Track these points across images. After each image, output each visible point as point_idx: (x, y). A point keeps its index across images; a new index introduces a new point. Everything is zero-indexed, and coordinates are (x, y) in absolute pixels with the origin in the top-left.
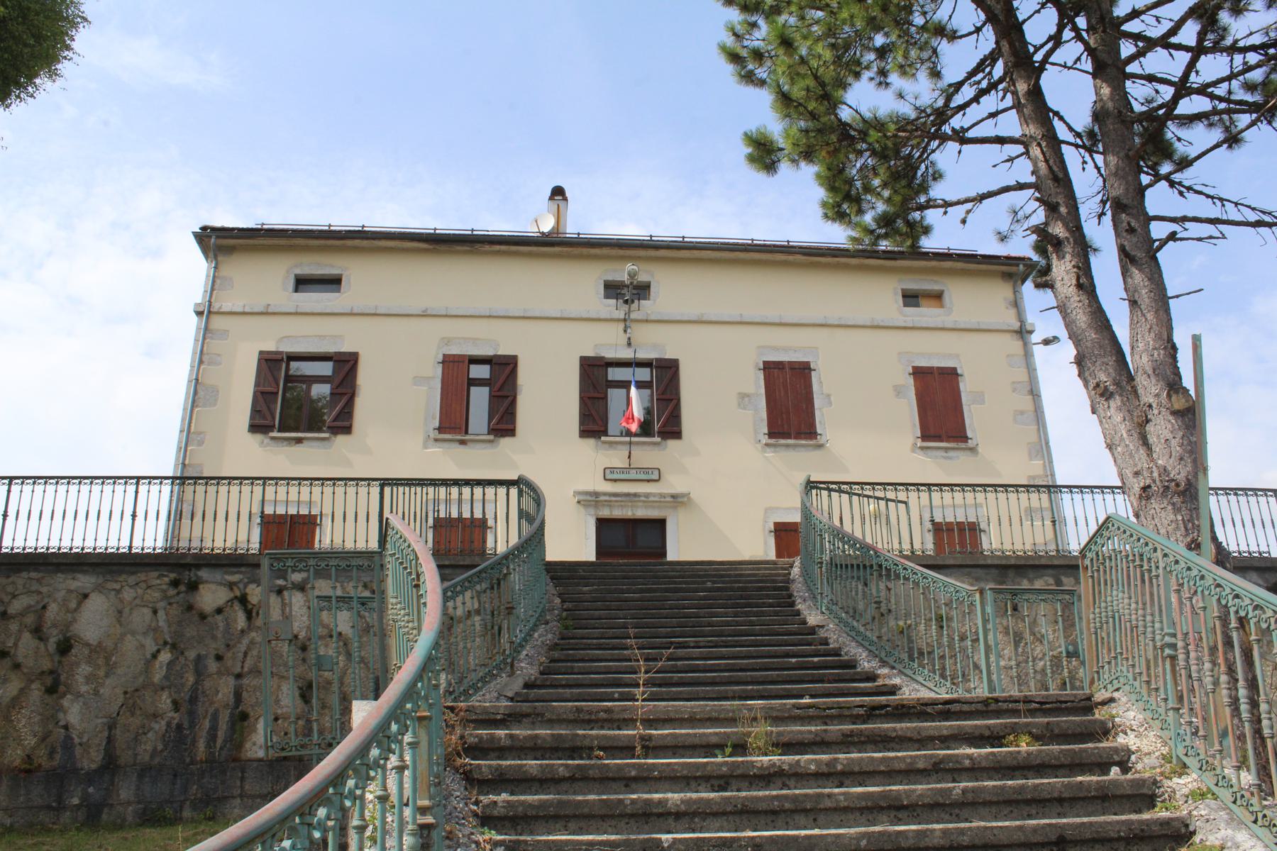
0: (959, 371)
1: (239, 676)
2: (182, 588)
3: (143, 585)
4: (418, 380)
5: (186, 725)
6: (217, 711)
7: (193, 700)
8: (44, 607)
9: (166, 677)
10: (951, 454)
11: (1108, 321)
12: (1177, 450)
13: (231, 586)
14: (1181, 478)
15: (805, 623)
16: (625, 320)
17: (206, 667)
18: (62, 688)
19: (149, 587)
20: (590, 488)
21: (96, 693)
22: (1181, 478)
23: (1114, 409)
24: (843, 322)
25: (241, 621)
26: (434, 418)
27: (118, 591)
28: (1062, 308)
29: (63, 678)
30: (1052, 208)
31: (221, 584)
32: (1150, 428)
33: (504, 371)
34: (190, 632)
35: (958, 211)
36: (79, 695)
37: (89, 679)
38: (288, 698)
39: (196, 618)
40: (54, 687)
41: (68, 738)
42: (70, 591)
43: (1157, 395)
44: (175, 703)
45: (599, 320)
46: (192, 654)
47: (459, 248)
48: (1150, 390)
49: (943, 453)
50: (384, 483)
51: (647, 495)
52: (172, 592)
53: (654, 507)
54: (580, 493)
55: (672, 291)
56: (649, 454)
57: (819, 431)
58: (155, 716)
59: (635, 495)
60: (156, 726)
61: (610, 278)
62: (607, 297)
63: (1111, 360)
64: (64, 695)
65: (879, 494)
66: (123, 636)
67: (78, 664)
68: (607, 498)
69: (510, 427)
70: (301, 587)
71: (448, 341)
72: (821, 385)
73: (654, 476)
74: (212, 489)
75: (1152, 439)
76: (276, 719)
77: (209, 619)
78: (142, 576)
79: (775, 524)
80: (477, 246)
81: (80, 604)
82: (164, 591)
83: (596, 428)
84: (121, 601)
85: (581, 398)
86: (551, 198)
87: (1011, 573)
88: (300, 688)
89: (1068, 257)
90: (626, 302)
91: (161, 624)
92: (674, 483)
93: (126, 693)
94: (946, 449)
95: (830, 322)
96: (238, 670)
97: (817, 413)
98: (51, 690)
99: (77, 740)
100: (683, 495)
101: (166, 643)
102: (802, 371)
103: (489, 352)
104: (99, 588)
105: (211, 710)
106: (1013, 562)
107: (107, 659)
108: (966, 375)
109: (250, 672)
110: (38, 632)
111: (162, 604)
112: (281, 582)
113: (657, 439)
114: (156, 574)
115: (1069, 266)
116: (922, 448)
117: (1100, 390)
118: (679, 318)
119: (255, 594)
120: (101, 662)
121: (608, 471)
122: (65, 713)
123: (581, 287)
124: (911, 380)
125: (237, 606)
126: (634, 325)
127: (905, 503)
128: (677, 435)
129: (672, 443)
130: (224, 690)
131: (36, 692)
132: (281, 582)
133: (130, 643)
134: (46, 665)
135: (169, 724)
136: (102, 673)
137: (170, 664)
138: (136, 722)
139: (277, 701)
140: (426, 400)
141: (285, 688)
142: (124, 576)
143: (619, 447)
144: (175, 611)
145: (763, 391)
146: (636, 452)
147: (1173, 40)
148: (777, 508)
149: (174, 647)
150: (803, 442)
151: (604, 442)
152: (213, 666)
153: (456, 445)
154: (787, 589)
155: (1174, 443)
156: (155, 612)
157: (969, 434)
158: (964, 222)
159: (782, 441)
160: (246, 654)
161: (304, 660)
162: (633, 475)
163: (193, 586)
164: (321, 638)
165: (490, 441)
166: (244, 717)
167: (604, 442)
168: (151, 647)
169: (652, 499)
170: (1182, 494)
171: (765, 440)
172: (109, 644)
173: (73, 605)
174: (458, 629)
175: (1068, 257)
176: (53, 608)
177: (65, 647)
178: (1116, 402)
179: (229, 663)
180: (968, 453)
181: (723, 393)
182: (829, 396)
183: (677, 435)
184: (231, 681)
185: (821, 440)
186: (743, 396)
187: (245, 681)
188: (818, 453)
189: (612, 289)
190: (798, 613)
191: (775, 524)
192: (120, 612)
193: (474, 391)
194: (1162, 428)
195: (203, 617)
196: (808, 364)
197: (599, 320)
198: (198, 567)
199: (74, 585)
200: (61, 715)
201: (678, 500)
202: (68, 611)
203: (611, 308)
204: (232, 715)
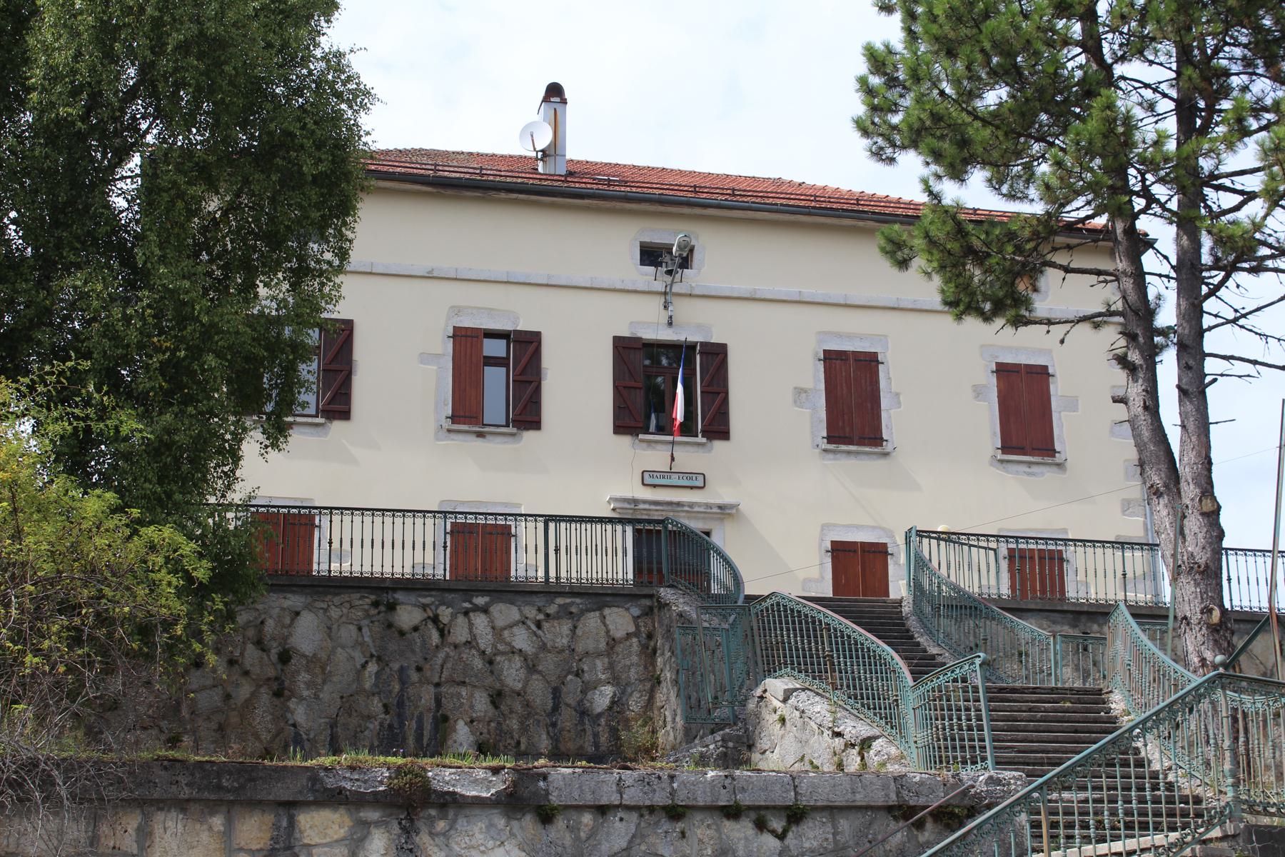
0: (1051, 371)
1: (437, 685)
2: (382, 608)
3: (347, 605)
4: (425, 358)
5: (396, 725)
6: (421, 713)
7: (401, 704)
8: (262, 623)
9: (376, 685)
10: (1035, 469)
11: (1165, 435)
12: (1202, 541)
13: (424, 607)
14: (1202, 562)
15: (925, 651)
16: (665, 293)
17: (408, 676)
18: (287, 693)
19: (352, 607)
20: (629, 495)
21: (317, 697)
22: (1202, 562)
23: (1162, 508)
24: (919, 307)
25: (435, 637)
26: (446, 405)
27: (325, 610)
28: (1132, 422)
29: (287, 683)
30: (1131, 337)
31: (415, 605)
32: (1186, 521)
33: (525, 350)
34: (392, 646)
35: (1058, 331)
36: (302, 699)
37: (309, 685)
38: (481, 703)
39: (396, 634)
40: (280, 693)
41: (297, 735)
42: (283, 609)
43: (1192, 500)
44: (385, 706)
45: (636, 292)
46: (396, 666)
47: (469, 194)
48: (1189, 491)
49: (1024, 468)
50: (548, 519)
51: (691, 505)
52: (373, 611)
53: (696, 518)
54: (616, 500)
55: (723, 257)
56: (692, 456)
57: (885, 437)
58: (369, 717)
59: (679, 504)
60: (371, 726)
61: (647, 240)
62: (643, 263)
63: (1163, 467)
64: (289, 699)
65: (982, 544)
66: (334, 648)
67: (298, 672)
68: (647, 506)
69: (535, 419)
70: (485, 610)
71: (457, 310)
72: (891, 380)
73: (697, 482)
74: (378, 520)
75: (1187, 531)
76: (472, 721)
77: (408, 636)
78: (346, 597)
79: (833, 542)
80: (492, 193)
81: (293, 620)
82: (366, 611)
83: (633, 424)
84: (330, 618)
85: (616, 388)
86: (546, 99)
87: (1083, 618)
88: (491, 696)
89: (1140, 381)
90: (669, 272)
91: (366, 639)
92: (719, 493)
93: (342, 697)
94: (1030, 464)
95: (903, 305)
96: (436, 680)
97: (884, 415)
98: (278, 694)
99: (304, 737)
100: (732, 506)
101: (372, 656)
102: (868, 364)
103: (506, 326)
104: (308, 607)
105: (416, 714)
106: (1085, 609)
107: (323, 669)
108: (1058, 375)
109: (447, 682)
110: (259, 643)
111: (366, 622)
112: (467, 605)
113: (700, 439)
114: (358, 595)
115: (1140, 389)
116: (1002, 461)
117: (1153, 490)
118: (728, 294)
119: (445, 613)
120: (317, 670)
121: (646, 475)
122: (292, 713)
123: (609, 247)
124: (994, 380)
125: (430, 625)
126: (675, 300)
127: (995, 550)
128: (724, 434)
129: (718, 445)
130: (426, 696)
131: (265, 696)
132: (467, 605)
133: (341, 655)
134: (271, 673)
135: (381, 724)
136: (320, 681)
137: (378, 674)
138: (354, 721)
139: (472, 707)
140: (434, 383)
141: (477, 695)
142: (329, 597)
143: (659, 447)
144: (377, 628)
145: (823, 386)
146: (680, 453)
147: (1239, 198)
148: (835, 525)
149: (379, 659)
150: (867, 449)
151: (642, 441)
152: (414, 676)
153: (473, 437)
154: (903, 625)
155: (1200, 536)
156: (360, 629)
157: (1058, 447)
158: (1062, 342)
159: (844, 447)
160: (442, 666)
161: (492, 672)
162: (675, 480)
163: (392, 607)
164: (503, 653)
165: (512, 435)
166: (445, 719)
167: (642, 441)
168: (359, 659)
169: (696, 509)
170: (1202, 573)
171: (824, 444)
172: (323, 655)
173: (287, 621)
174: (619, 648)
175: (1140, 381)
176: (270, 624)
177: (285, 657)
178: (1164, 500)
179: (429, 674)
180: (1055, 469)
181: (774, 387)
182: (897, 395)
183: (724, 434)
184: (432, 689)
185: (888, 447)
186: (800, 391)
187: (443, 689)
188: (881, 463)
189: (651, 255)
190: (918, 644)
191: (833, 542)
192: (329, 628)
193: (489, 371)
194: (1194, 524)
195: (402, 633)
196: (875, 354)
197: (636, 292)
198: (395, 590)
199: (287, 603)
200: (289, 715)
201: (725, 512)
202: (283, 626)
203: (647, 276)
204: (435, 718)
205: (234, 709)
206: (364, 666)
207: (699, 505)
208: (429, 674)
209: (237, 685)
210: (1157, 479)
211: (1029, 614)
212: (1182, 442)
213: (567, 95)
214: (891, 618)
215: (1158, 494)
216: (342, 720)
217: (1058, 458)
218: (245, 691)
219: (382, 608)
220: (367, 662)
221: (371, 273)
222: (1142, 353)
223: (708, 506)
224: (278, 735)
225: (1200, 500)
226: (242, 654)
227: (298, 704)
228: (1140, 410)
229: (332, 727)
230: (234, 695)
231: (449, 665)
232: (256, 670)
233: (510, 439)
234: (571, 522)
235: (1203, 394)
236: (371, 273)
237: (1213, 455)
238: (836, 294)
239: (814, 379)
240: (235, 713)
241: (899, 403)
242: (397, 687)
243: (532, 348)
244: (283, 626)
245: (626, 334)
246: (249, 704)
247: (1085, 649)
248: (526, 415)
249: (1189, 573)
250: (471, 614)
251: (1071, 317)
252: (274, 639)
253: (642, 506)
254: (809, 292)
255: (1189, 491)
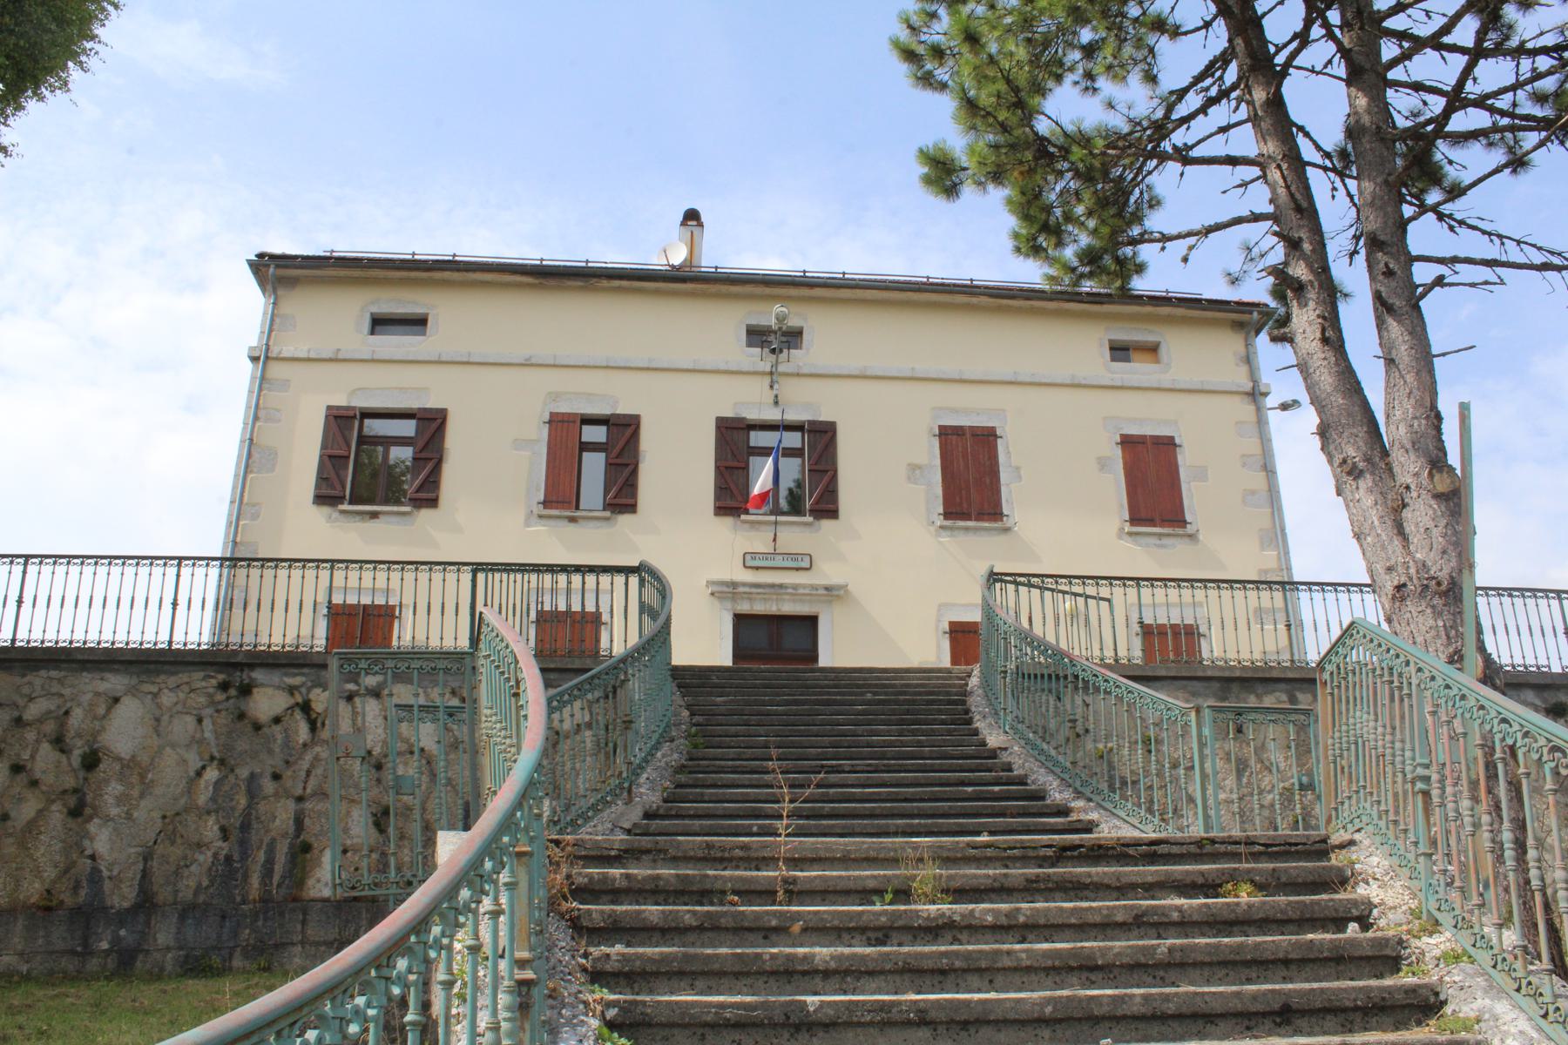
0: (1177, 441)
1: (300, 799)
2: (233, 692)
3: (186, 688)
4: (519, 444)
5: (236, 857)
6: (273, 840)
7: (245, 827)
8: (67, 713)
9: (213, 799)
10: (1165, 541)
11: (1358, 383)
13: (291, 690)
14: (1444, 575)
15: (984, 744)
16: (771, 373)
17: (260, 787)
18: (88, 811)
19: (192, 691)
20: (727, 577)
21: (129, 816)
22: (1444, 575)
23: (1364, 491)
26: (538, 490)
27: (155, 695)
28: (1303, 367)
29: (89, 798)
31: (278, 688)
33: (623, 435)
35: (1179, 247)
37: (121, 800)
38: (359, 826)
39: (249, 729)
41: (95, 871)
42: (98, 694)
43: (1416, 475)
44: (223, 830)
46: (244, 773)
48: (1408, 467)
50: (477, 568)
51: (795, 587)
52: (220, 696)
55: (830, 338)
56: (796, 535)
58: (199, 845)
59: (781, 586)
60: (201, 858)
61: (754, 322)
64: (91, 818)
66: (161, 749)
67: (107, 781)
68: (747, 589)
70: (376, 693)
71: (555, 396)
72: (1008, 455)
73: (803, 562)
76: (345, 852)
78: (184, 677)
79: (951, 623)
81: (109, 710)
82: (210, 696)
84: (159, 706)
86: (684, 223)
87: (1235, 687)
88: (375, 815)
89: (1312, 304)
90: (773, 351)
92: (828, 572)
94: (1160, 535)
95: (1020, 379)
96: (299, 792)
97: (1003, 489)
98: (76, 812)
99: (106, 873)
101: (212, 758)
102: (986, 439)
104: (133, 691)
105: (266, 840)
106: (1238, 674)
107: (142, 777)
109: (314, 795)
110: (59, 742)
111: (209, 711)
113: (809, 519)
114: (202, 674)
115: (1313, 315)
117: (1347, 468)
119: (320, 700)
120: (135, 779)
122: (92, 840)
123: (717, 332)
124: (1118, 452)
125: (298, 715)
126: (782, 380)
127: (1108, 600)
129: (827, 524)
130: (282, 815)
131: (57, 814)
132: (351, 687)
133: (169, 758)
134: (69, 782)
135: (215, 855)
136: (135, 793)
137: (218, 784)
138: (176, 852)
139: (346, 830)
140: (529, 467)
142: (163, 677)
143: (763, 527)
144: (223, 719)
145: (938, 462)
147: (1446, 40)
148: (954, 605)
149: (222, 762)
152: (269, 786)
153: (566, 522)
154: (964, 703)
156: (200, 721)
157: (1188, 518)
158: (1185, 260)
160: (308, 773)
162: (779, 562)
163: (246, 690)
166: (307, 848)
168: (194, 762)
169: (801, 591)
171: (940, 521)
172: (144, 759)
173: (101, 711)
174: (565, 746)
175: (1312, 304)
177: (91, 761)
178: (1366, 482)
179: (289, 784)
181: (885, 465)
182: (1018, 468)
183: (833, 514)
184: (291, 805)
185: (1007, 522)
186: (913, 468)
187: (308, 805)
188: (1002, 539)
189: (757, 336)
190: (976, 732)
191: (951, 623)
192: (158, 720)
193: (588, 457)
194: (1422, 514)
195: (257, 727)
198: (252, 666)
199: (103, 686)
200: (86, 843)
201: (833, 593)
202: (95, 718)
203: (754, 358)
204: (291, 846)
205: (11, 835)
206: (199, 774)
207: (804, 586)
208: (289, 784)
209: (20, 800)
210: (1352, 452)
211: (1165, 683)
212: (1389, 387)
213: (703, 219)
214: (948, 693)
215: (1355, 473)
216: (159, 849)
217: (1190, 529)
218: (28, 809)
219: (233, 692)
220: (204, 768)
221: (468, 363)
222: (1310, 266)
223: (814, 587)
224: (66, 871)
225: (1431, 475)
226: (33, 757)
227: (100, 826)
228: (1315, 346)
229: (145, 860)
230: (13, 814)
231: (319, 771)
232: (48, 779)
233: (604, 523)
234: (529, 571)
235: (1417, 308)
236: (468, 363)
237: (1440, 407)
238: (950, 368)
239: (930, 455)
240: (11, 840)
241: (1020, 477)
242: (243, 801)
243: (629, 431)
244: (95, 718)
245: (730, 414)
246: (32, 827)
247: (1239, 730)
248: (622, 496)
249: (1422, 595)
250: (357, 700)
251: (1197, 227)
252: (79, 735)
253: (741, 589)
254: (924, 367)
255: (1408, 467)
